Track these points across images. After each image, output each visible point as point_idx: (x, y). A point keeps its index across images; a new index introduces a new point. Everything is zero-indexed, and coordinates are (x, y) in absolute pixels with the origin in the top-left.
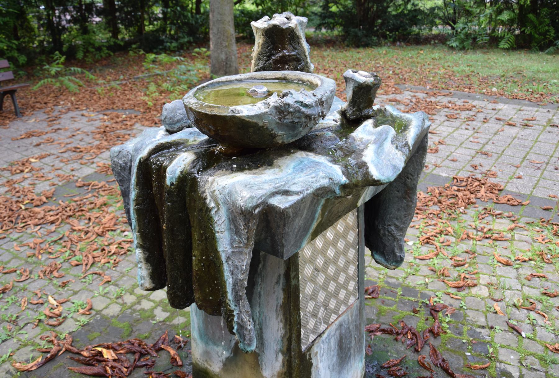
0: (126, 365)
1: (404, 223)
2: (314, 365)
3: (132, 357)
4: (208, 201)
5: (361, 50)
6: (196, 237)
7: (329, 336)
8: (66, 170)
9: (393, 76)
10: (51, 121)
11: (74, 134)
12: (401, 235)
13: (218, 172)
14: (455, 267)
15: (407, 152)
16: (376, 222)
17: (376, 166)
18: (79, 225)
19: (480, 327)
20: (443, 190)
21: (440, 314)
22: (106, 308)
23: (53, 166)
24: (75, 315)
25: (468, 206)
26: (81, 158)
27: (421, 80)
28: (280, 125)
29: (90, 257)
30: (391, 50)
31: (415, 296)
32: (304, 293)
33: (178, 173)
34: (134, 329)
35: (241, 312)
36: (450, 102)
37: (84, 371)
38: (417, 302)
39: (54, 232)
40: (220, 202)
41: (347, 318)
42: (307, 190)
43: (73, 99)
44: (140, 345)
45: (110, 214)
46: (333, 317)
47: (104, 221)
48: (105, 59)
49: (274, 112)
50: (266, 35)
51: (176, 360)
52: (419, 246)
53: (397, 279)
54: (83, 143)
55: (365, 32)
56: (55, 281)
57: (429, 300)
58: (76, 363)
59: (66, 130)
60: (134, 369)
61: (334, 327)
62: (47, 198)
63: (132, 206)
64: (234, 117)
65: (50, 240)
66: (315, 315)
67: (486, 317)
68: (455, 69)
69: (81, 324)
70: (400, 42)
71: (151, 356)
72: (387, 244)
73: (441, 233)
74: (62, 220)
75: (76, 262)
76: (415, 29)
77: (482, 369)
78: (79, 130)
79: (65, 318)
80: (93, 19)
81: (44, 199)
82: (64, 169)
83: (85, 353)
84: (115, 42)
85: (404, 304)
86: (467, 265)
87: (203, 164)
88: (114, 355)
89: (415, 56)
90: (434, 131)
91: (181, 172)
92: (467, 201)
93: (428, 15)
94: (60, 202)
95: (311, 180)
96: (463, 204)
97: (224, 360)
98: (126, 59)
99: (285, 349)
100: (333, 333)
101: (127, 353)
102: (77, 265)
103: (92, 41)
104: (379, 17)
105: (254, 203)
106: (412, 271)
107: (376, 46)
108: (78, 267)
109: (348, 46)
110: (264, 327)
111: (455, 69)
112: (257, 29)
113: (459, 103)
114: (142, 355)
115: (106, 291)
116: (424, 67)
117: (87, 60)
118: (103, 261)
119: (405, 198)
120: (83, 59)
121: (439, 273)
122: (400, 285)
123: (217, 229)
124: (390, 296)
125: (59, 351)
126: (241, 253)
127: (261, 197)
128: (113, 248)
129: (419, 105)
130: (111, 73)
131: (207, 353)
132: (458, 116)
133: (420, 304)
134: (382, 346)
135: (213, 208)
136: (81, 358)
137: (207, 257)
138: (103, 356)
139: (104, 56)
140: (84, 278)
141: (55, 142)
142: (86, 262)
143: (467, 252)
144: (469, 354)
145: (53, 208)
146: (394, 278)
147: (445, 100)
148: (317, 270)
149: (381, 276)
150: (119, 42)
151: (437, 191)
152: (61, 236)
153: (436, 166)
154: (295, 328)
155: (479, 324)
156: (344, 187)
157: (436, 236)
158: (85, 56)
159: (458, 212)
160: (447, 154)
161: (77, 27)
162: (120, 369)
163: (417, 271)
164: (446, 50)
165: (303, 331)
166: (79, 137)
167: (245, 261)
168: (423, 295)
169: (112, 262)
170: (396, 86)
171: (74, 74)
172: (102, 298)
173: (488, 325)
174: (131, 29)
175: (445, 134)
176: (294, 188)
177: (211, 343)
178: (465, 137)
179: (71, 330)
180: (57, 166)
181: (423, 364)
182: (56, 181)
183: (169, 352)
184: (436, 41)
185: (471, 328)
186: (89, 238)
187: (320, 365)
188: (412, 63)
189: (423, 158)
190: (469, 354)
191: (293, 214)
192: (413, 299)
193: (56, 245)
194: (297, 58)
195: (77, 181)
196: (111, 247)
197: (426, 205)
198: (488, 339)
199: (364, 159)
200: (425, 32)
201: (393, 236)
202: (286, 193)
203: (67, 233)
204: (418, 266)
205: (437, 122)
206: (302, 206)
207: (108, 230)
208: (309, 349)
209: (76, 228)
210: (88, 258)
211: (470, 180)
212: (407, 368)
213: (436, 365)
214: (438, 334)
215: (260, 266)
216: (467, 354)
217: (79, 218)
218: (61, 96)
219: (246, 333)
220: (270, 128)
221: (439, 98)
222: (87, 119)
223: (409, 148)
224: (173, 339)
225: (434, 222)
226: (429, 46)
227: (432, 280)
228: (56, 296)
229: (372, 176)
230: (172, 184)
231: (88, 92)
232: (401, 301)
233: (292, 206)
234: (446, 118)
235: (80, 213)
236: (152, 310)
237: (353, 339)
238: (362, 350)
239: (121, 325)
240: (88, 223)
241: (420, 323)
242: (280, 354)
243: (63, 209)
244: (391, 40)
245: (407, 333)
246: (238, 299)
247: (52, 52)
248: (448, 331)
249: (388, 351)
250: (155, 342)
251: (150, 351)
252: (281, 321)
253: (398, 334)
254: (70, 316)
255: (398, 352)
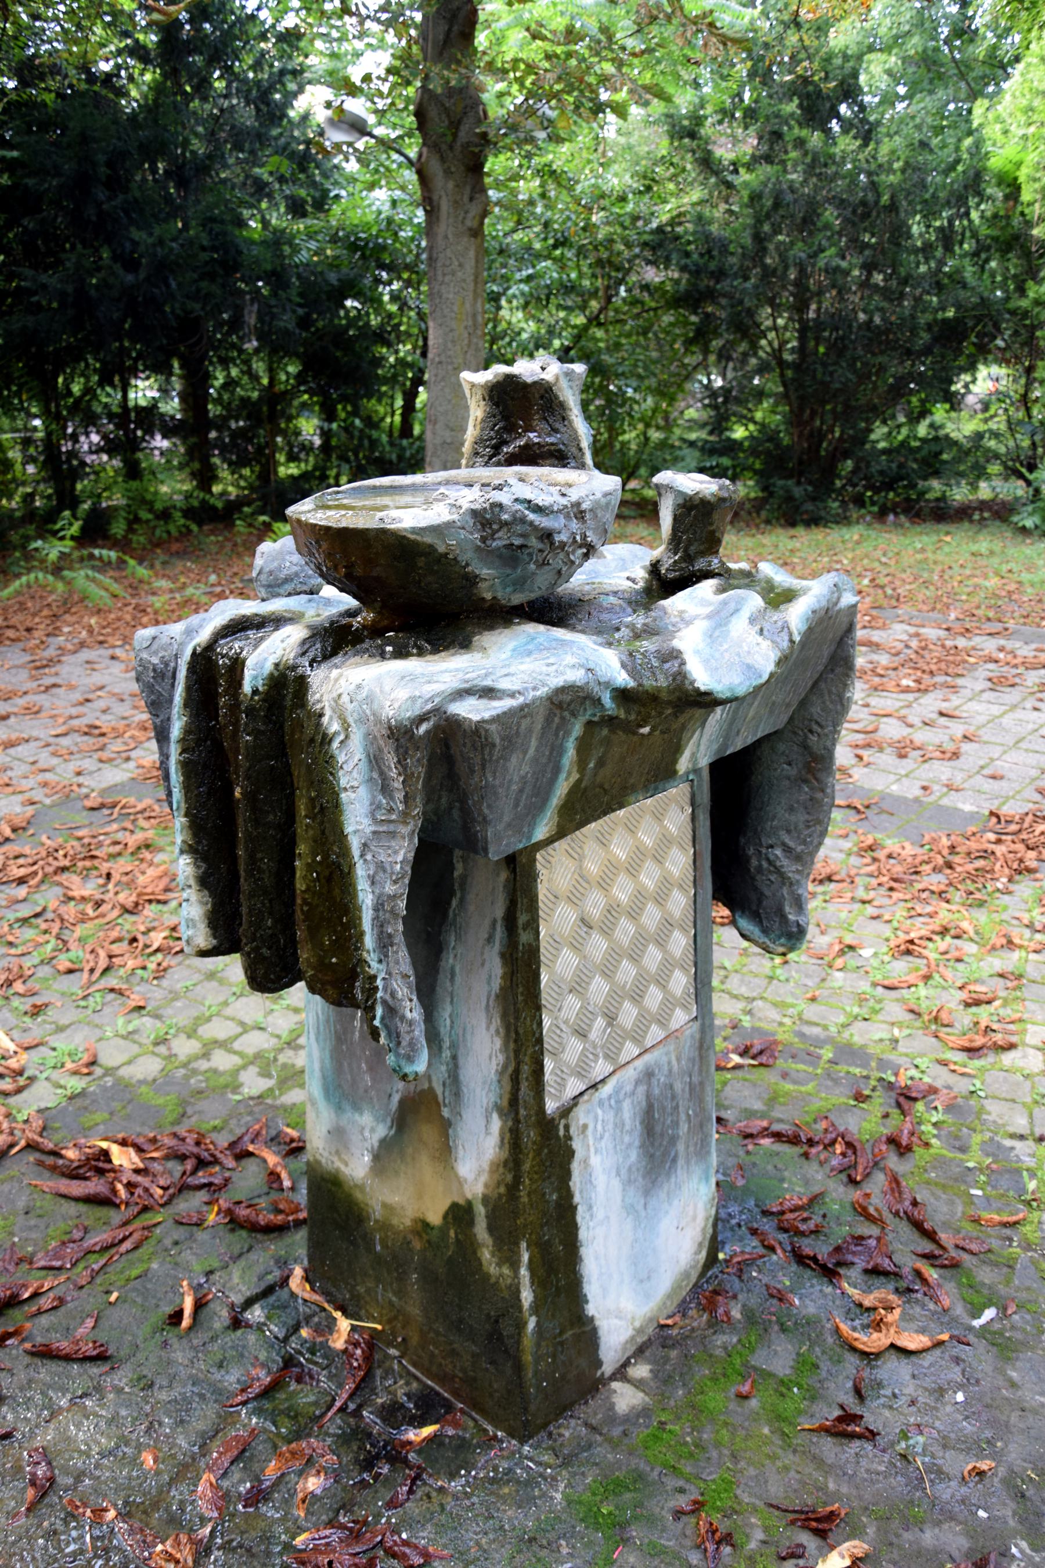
0: (162, 1183)
1: (804, 842)
2: (579, 1156)
3: (177, 1168)
4: (325, 720)
5: (800, 531)
6: (302, 809)
7: (617, 1091)
8: (65, 772)
9: (871, 591)
10: (37, 668)
11: (90, 696)
12: (798, 871)
13: (352, 660)
14: (968, 1005)
15: (785, 644)
16: (742, 840)
17: (706, 662)
18: (84, 887)
19: (1012, 1136)
20: (960, 839)
21: (920, 1106)
22: (129, 1063)
23: (34, 763)
24: (55, 1075)
25: (1017, 877)
26: (102, 749)
27: (938, 599)
28: (484, 552)
29: (102, 954)
30: (873, 534)
31: (865, 1065)
32: (552, 973)
33: (268, 667)
34: (190, 1111)
35: (390, 971)
36: (1001, 649)
37: (63, 1190)
38: (867, 1077)
39: (25, 900)
40: (350, 720)
41: (665, 1059)
42: (534, 689)
43: (93, 621)
44: (198, 1143)
45: (158, 866)
46: (630, 1049)
47: (141, 880)
48: (177, 540)
49: (471, 522)
50: (491, 398)
51: (279, 1176)
52: (887, 958)
53: (825, 1028)
54: (108, 717)
55: (810, 488)
56: (16, 1002)
57: (896, 1074)
58: (47, 1174)
59: (71, 687)
60: (180, 1191)
61: (630, 1074)
62: (14, 830)
63: (174, 751)
64: (384, 531)
65: (11, 916)
66: (582, 1034)
67: (1031, 1116)
68: (1025, 577)
69: (69, 1093)
70: (896, 514)
71: (223, 1167)
72: (767, 893)
73: (944, 931)
74: (45, 875)
75: (69, 965)
76: (936, 486)
77: (1005, 1225)
78: (101, 688)
79: (32, 1079)
80: (154, 444)
81: (8, 832)
82: (58, 770)
83: (71, 1154)
84: (203, 502)
85: (836, 1081)
86: (997, 1003)
87: (324, 649)
88: (136, 1159)
89: (931, 547)
90: (957, 713)
91: (277, 665)
92: (1015, 866)
93: (968, 453)
94: (44, 838)
95: (544, 669)
96: (1007, 871)
97: (376, 1145)
98: (227, 539)
99: (505, 1103)
100: (629, 1088)
101: (167, 1158)
102: (70, 971)
103: (149, 497)
104: (846, 455)
105: (417, 710)
106: (864, 1012)
107: (837, 523)
108: (71, 976)
109: (768, 522)
110: (461, 1052)
111: (1025, 577)
112: (473, 385)
113: (1026, 651)
114: (201, 1164)
115: (131, 1028)
116: (949, 572)
117: (135, 538)
118: (131, 964)
119: (805, 781)
120: (125, 537)
121: (926, 1018)
122: (830, 1040)
123: (343, 782)
124: (803, 1062)
125: (12, 1146)
126: (392, 835)
127: (431, 699)
128: (157, 939)
129: (925, 653)
130: (190, 570)
131: (338, 1134)
132: (1017, 680)
133: (873, 1083)
134: (770, 1167)
135: (336, 733)
136: (61, 1162)
137: (326, 857)
138: (110, 1161)
139: (174, 532)
140: (85, 998)
141: (43, 714)
142: (92, 964)
143: (1001, 975)
144: (979, 1193)
145: (27, 850)
146: (817, 1025)
147: (990, 645)
148: (585, 922)
149: (787, 1021)
150: (212, 501)
151: (945, 842)
152: (38, 909)
153: (950, 787)
154: (530, 1051)
155: (1011, 1130)
156: (623, 695)
157: (930, 939)
158: (130, 530)
159: (990, 889)
160: (982, 763)
161: (117, 463)
162: (146, 1190)
163: (876, 1012)
164: (1009, 534)
165: (549, 1064)
166: (102, 704)
167: (400, 853)
168: (883, 1064)
169: (152, 966)
170: (874, 612)
171: (105, 566)
172: (121, 1042)
173: (1032, 1134)
174: (246, 472)
175: (981, 719)
176: (504, 684)
177: (347, 1107)
178: (1031, 726)
179: (43, 1105)
180: (41, 765)
181: (865, 1209)
182: (38, 795)
183: (265, 1161)
184: (986, 515)
185: (992, 1139)
186: (103, 915)
187: (595, 1161)
188: (920, 562)
189: (845, 685)
190: (979, 1193)
191: (502, 739)
192: (857, 1071)
193: (24, 929)
194: (560, 451)
195: (87, 796)
196: (152, 934)
197: (916, 873)
198: (1029, 1162)
199: (676, 643)
200: (960, 494)
201: (778, 871)
202: (488, 693)
203: (53, 904)
204: (879, 1001)
205: (966, 693)
206: (525, 723)
207: (150, 901)
208: (566, 1112)
209: (76, 893)
210: (97, 956)
211: (1029, 819)
212: (824, 1216)
213: (897, 1214)
214: (909, 1149)
215: (454, 903)
216: (973, 1192)
217: (85, 875)
218: (67, 617)
219: (403, 1028)
220: (463, 559)
221: (977, 641)
222: (123, 666)
223: (791, 634)
224: (278, 1135)
225: (929, 909)
226: (966, 524)
227: (907, 1032)
228: (15, 1034)
229: (692, 682)
230: (255, 692)
231: (130, 608)
232: (828, 1075)
233: (496, 719)
234: (989, 684)
235: (88, 863)
236: (237, 1071)
237: (683, 1117)
238: (708, 1153)
239: (161, 1101)
240: (104, 885)
241: (868, 1124)
242: (495, 1116)
243: (49, 854)
244: (875, 509)
245: (833, 1142)
246: (384, 943)
247: (51, 515)
248: (933, 1141)
249: (782, 1180)
250: (232, 1139)
251: (219, 1155)
252: (497, 1032)
253: (811, 1143)
254: (45, 1075)
255: (807, 1182)
